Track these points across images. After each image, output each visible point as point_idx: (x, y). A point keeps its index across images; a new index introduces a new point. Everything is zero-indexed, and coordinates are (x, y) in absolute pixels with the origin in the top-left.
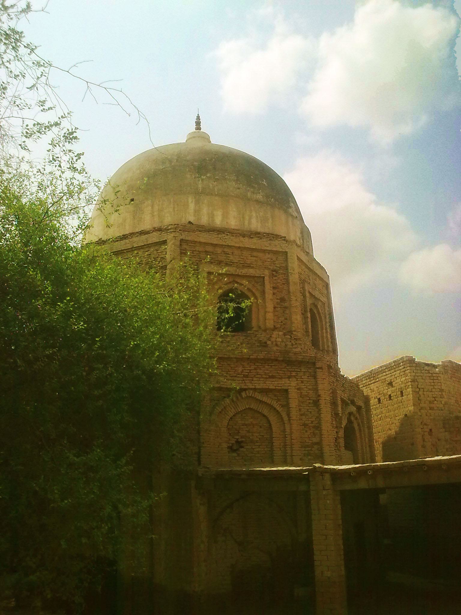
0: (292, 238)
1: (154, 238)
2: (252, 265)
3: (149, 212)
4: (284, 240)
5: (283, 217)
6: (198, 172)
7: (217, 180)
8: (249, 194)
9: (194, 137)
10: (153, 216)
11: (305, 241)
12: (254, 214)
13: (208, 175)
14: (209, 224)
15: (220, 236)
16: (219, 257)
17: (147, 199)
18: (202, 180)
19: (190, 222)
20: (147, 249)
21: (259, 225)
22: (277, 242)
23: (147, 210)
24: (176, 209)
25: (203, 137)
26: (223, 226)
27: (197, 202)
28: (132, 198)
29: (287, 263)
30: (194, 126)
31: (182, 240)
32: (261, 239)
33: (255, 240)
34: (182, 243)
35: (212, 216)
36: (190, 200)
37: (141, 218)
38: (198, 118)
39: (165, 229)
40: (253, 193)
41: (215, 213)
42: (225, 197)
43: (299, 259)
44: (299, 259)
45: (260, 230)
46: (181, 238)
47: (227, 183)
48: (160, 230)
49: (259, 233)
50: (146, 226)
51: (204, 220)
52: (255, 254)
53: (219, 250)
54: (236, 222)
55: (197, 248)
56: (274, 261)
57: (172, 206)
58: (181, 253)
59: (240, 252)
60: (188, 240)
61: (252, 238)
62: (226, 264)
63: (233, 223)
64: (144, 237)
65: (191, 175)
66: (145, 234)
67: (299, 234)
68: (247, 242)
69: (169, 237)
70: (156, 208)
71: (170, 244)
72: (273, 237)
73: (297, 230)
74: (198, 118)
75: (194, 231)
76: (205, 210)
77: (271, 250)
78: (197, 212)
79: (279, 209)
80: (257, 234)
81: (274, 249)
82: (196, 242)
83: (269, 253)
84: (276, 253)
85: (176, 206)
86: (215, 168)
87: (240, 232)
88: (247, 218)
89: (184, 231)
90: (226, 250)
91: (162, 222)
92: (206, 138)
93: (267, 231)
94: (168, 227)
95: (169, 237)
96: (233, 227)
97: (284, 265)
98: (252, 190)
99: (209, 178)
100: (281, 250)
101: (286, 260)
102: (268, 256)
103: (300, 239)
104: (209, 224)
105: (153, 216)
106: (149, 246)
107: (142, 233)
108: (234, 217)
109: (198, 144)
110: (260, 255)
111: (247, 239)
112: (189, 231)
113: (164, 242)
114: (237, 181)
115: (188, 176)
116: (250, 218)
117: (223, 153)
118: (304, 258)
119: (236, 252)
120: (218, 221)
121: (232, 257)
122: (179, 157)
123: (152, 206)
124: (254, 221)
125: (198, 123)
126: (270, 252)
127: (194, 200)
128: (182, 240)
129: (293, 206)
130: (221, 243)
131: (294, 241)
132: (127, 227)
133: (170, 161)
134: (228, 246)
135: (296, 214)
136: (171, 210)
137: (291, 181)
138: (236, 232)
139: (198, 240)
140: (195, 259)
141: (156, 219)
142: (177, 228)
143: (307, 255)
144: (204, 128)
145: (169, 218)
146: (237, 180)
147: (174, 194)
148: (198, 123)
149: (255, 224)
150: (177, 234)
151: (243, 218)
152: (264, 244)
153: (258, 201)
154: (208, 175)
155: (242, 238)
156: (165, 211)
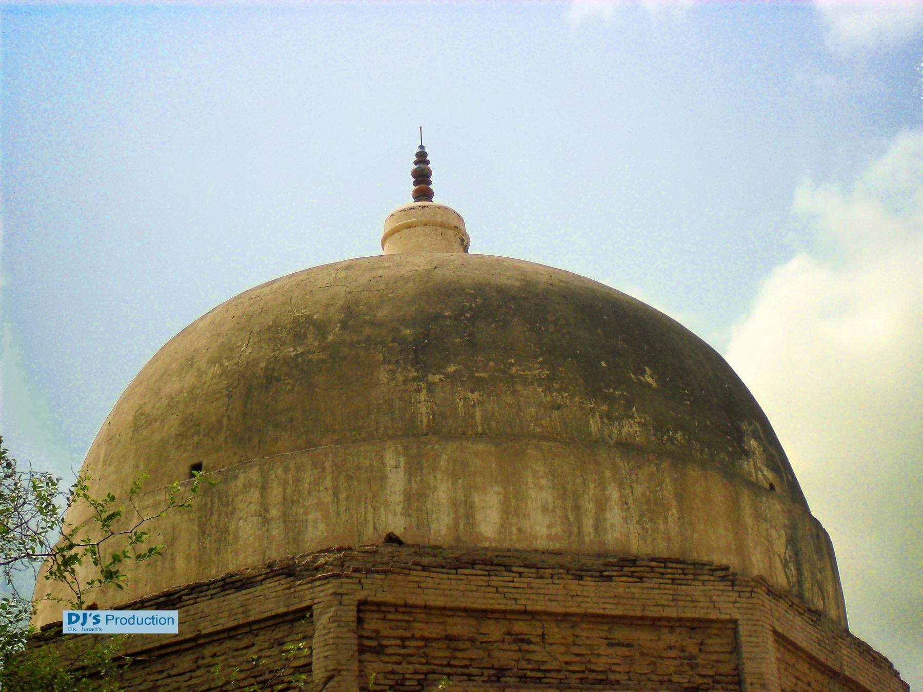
0: (757, 564)
1: (269, 600)
2: (613, 677)
3: (254, 508)
4: (722, 579)
5: (718, 493)
6: (415, 363)
7: (478, 384)
8: (594, 425)
9: (409, 226)
10: (266, 521)
11: (806, 567)
12: (614, 493)
13: (451, 369)
14: (458, 539)
15: (496, 580)
16: (496, 654)
17: (244, 463)
18: (431, 388)
19: (392, 539)
20: (246, 641)
21: (634, 529)
22: (696, 589)
23: (247, 503)
24: (343, 496)
25: (442, 225)
26: (507, 545)
27: (414, 467)
28: (194, 461)
29: (739, 658)
30: (409, 186)
31: (362, 605)
32: (641, 578)
33: (620, 587)
34: (368, 616)
35: (465, 511)
36: (390, 458)
37: (227, 530)
38: (422, 157)
39: (307, 568)
40: (609, 417)
41: (476, 498)
42: (509, 440)
43: (780, 638)
44: (780, 638)
45: (637, 546)
46: (361, 595)
47: (514, 392)
48: (288, 571)
49: (634, 561)
50: (242, 557)
51: (441, 527)
52: (621, 634)
53: (494, 630)
54: (550, 526)
55: (420, 628)
56: (691, 657)
57: (328, 482)
58: (362, 650)
59: (569, 632)
60: (385, 604)
61: (609, 578)
62: (523, 678)
63: (540, 528)
64: (236, 598)
65: (393, 372)
66: (238, 589)
67: (780, 547)
68: (592, 597)
69: (317, 593)
70: (276, 491)
71: (324, 619)
72: (680, 568)
73: (774, 533)
74: (422, 157)
75: (405, 570)
76: (442, 492)
77: (679, 619)
78: (415, 499)
79: (703, 465)
80: (626, 565)
81: (689, 614)
82: (409, 608)
83: (672, 629)
84: (696, 625)
85: (343, 483)
86: (472, 343)
87: (566, 560)
88: (589, 507)
89: (369, 571)
90: (519, 627)
91: (296, 541)
92: (452, 230)
93: (661, 549)
94: (315, 559)
95: (317, 593)
96: (541, 544)
97: (726, 668)
98: (605, 408)
99: (452, 378)
100: (713, 615)
101: (735, 648)
102: (669, 638)
103: (785, 565)
104: (458, 539)
105: (266, 521)
106: (251, 628)
107: (234, 583)
108: (545, 509)
109: (424, 258)
110: (644, 637)
111: (590, 586)
112: (385, 572)
113: (303, 614)
114: (547, 383)
115: (383, 377)
116: (601, 505)
117: (502, 291)
118: (801, 633)
119: (556, 633)
120: (489, 525)
121: (539, 654)
122: (351, 314)
123: (264, 488)
124: (614, 515)
125: (422, 177)
126: (673, 624)
127: (402, 460)
128: (362, 605)
129: (758, 451)
130: (499, 603)
131: (760, 581)
132: (180, 563)
133: (321, 328)
134: (525, 612)
135: (770, 475)
136: (327, 498)
137: (755, 356)
138: (552, 560)
139: (420, 601)
140: (411, 668)
141: (277, 531)
142: (346, 561)
143: (815, 623)
144: (443, 193)
145: (322, 527)
146: (551, 378)
147: (337, 442)
148: (422, 177)
149: (619, 525)
150: (347, 585)
151: (577, 508)
152: (649, 597)
153: (625, 447)
154: (451, 369)
155: (574, 585)
156: (308, 503)
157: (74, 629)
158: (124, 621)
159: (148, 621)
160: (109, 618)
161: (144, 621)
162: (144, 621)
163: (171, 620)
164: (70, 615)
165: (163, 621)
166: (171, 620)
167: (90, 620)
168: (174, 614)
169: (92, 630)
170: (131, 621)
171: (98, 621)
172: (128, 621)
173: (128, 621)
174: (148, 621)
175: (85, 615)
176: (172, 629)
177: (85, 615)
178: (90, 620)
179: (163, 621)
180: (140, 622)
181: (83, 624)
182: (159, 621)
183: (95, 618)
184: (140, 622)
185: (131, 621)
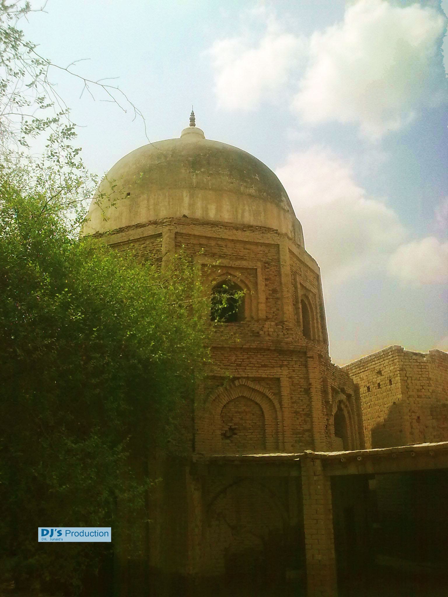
0: (284, 231)
1: (150, 231)
2: (245, 258)
3: (145, 206)
4: (276, 233)
5: (275, 211)
6: (192, 167)
7: (211, 175)
8: (242, 189)
10: (149, 209)
12: (247, 208)
13: (202, 170)
14: (203, 217)
15: (214, 229)
16: (213, 249)
17: (143, 193)
18: (197, 175)
19: (184, 216)
20: (143, 242)
21: (252, 218)
22: (269, 235)
23: (143, 204)
24: (171, 203)
26: (217, 220)
27: (192, 196)
28: (128, 192)
29: (279, 255)
31: (176, 233)
32: (254, 232)
33: (248, 233)
34: (177, 236)
35: (206, 210)
36: (185, 194)
37: (137, 211)
39: (161, 222)
40: (246, 187)
41: (209, 206)
42: (219, 191)
43: (290, 251)
44: (290, 251)
45: (252, 223)
46: (176, 231)
47: (220, 178)
48: (155, 223)
49: (252, 226)
50: (142, 219)
51: (199, 214)
52: (248, 246)
53: (213, 243)
54: (229, 215)
55: (192, 241)
56: (266, 254)
57: (167, 199)
58: (176, 246)
59: (233, 245)
60: (183, 233)
61: (245, 231)
62: (220, 256)
63: (226, 216)
64: (140, 230)
65: (186, 170)
66: (141, 228)
67: (290, 227)
68: (240, 235)
69: (164, 230)
70: (152, 201)
71: (166, 236)
72: (265, 230)
73: (289, 223)
75: (188, 224)
76: (199, 204)
77: (263, 243)
78: (192, 206)
79: (271, 203)
80: (250, 228)
81: (267, 242)
82: (190, 235)
83: (261, 246)
84: (268, 245)
85: (171, 200)
86: (209, 163)
87: (233, 225)
88: (240, 211)
89: (179, 224)
90: (219, 243)
91: (157, 215)
93: (259, 224)
94: (163, 220)
95: (164, 230)
96: (226, 221)
97: (276, 257)
98: (245, 184)
99: (203, 173)
100: (273, 243)
101: (278, 252)
102: (260, 248)
103: (291, 232)
104: (203, 217)
105: (149, 209)
106: (145, 239)
107: (138, 226)
108: (228, 211)
110: (253, 247)
111: (240, 232)
112: (183, 225)
113: (160, 235)
114: (230, 175)
115: (183, 171)
116: (243, 211)
117: (217, 149)
118: (295, 250)
119: (230, 245)
120: (212, 215)
121: (225, 250)
122: (174, 152)
123: (148, 200)
124: (247, 214)
126: (262, 244)
127: (188, 194)
128: (176, 233)
129: (285, 200)
130: (214, 235)
131: (286, 234)
132: (124, 221)
133: (166, 157)
134: (222, 239)
135: (288, 208)
136: (166, 204)
138: (229, 225)
139: (193, 233)
140: (190, 252)
141: (152, 212)
142: (172, 221)
143: (298, 248)
145: (165, 212)
146: (230, 175)
147: (169, 188)
149: (248, 218)
150: (172, 227)
151: (237, 211)
152: (257, 237)
153: (250, 196)
154: (202, 170)
155: (235, 231)
156: (161, 205)
157: (45, 539)
158: (77, 534)
159: (92, 534)
160: (67, 532)
161: (89, 534)
162: (89, 534)
163: (106, 533)
164: (43, 530)
165: (101, 534)
166: (106, 533)
167: (56, 534)
168: (109, 530)
169: (57, 540)
170: (82, 534)
171: (61, 534)
172: (79, 534)
173: (79, 534)
174: (92, 534)
175: (52, 530)
176: (108, 539)
177: (52, 530)
178: (56, 534)
179: (101, 534)
180: (87, 535)
181: (51, 536)
182: (99, 534)
183: (58, 532)
184: (87, 535)
185: (82, 534)
